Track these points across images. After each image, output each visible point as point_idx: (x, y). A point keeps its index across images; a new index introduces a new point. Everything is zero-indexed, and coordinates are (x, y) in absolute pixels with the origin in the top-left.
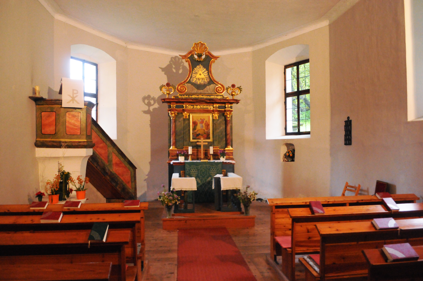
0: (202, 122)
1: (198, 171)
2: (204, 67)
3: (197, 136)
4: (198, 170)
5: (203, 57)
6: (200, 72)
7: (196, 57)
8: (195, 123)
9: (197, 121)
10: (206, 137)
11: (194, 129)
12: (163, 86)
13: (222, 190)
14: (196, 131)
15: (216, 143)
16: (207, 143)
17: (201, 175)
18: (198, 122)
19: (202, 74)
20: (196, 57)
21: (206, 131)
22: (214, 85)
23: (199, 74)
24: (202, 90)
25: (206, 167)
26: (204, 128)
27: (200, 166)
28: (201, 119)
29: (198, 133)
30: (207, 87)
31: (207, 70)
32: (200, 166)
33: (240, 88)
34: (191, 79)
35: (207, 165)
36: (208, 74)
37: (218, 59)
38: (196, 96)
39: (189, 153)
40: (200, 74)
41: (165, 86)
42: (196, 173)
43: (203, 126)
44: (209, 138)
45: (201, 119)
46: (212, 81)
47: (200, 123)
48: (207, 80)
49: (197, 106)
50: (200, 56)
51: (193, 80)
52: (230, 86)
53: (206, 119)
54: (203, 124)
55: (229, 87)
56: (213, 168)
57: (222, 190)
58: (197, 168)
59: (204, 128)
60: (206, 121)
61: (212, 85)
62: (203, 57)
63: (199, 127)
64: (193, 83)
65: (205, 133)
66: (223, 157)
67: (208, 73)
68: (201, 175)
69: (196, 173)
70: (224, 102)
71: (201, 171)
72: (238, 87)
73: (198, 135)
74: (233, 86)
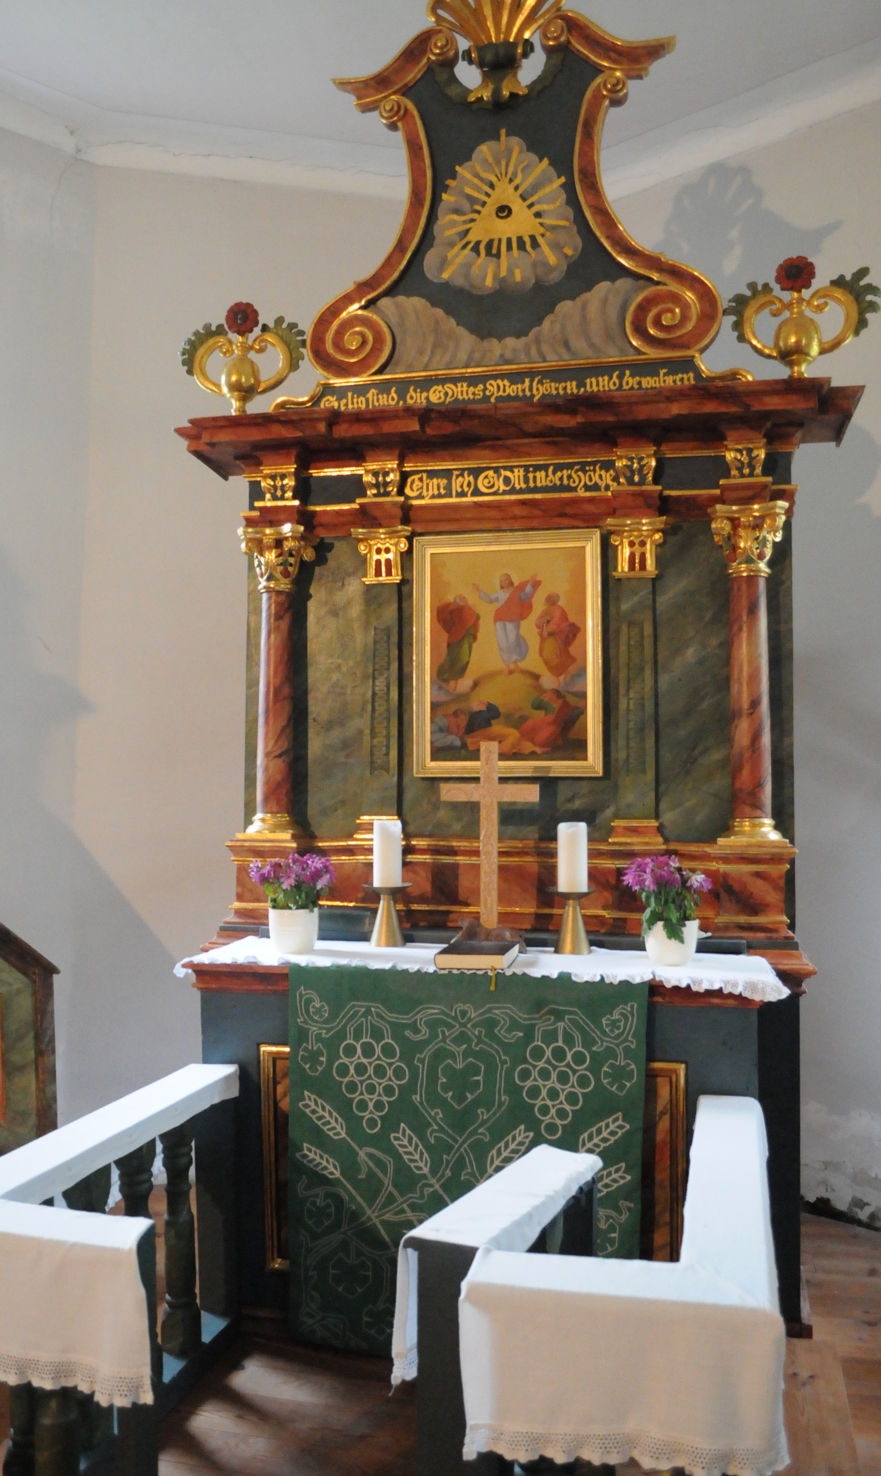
0: (516, 607)
1: (408, 1057)
2: (537, 145)
3: (466, 729)
4: (410, 1050)
5: (530, 70)
6: (505, 193)
7: (469, 76)
8: (455, 621)
9: (472, 600)
10: (545, 733)
11: (449, 668)
12: (209, 334)
13: (471, 1450)
14: (464, 684)
15: (635, 791)
16: (531, 794)
17: (435, 1100)
18: (486, 612)
19: (517, 206)
20: (469, 76)
21: (549, 681)
22: (623, 283)
23: (490, 209)
24: (520, 333)
25: (490, 1024)
26: (533, 662)
27: (433, 1011)
28: (507, 583)
29: (477, 704)
30: (565, 307)
31: (562, 165)
32: (433, 1011)
33: (856, 290)
34: (430, 259)
35: (503, 1011)
36: (572, 201)
37: (657, 68)
38: (462, 392)
39: (563, 885)
40: (504, 211)
41: (220, 331)
42: (390, 1079)
43: (521, 645)
44: (579, 748)
45: (507, 583)
46: (597, 255)
47: (500, 616)
48: (556, 247)
49: (476, 472)
50: (500, 61)
51: (443, 263)
52: (768, 275)
53: (555, 583)
54: (529, 628)
55: (758, 291)
56: (550, 1036)
57: (471, 1450)
58: (397, 1030)
59: (533, 662)
60: (552, 600)
61: (604, 287)
62: (530, 70)
63: (489, 650)
64: (446, 286)
65: (539, 706)
66: (674, 932)
67: (569, 187)
68: (435, 1100)
69: (390, 1079)
70: (717, 414)
71: (439, 1056)
72: (839, 282)
73: (480, 722)
74: (797, 273)
